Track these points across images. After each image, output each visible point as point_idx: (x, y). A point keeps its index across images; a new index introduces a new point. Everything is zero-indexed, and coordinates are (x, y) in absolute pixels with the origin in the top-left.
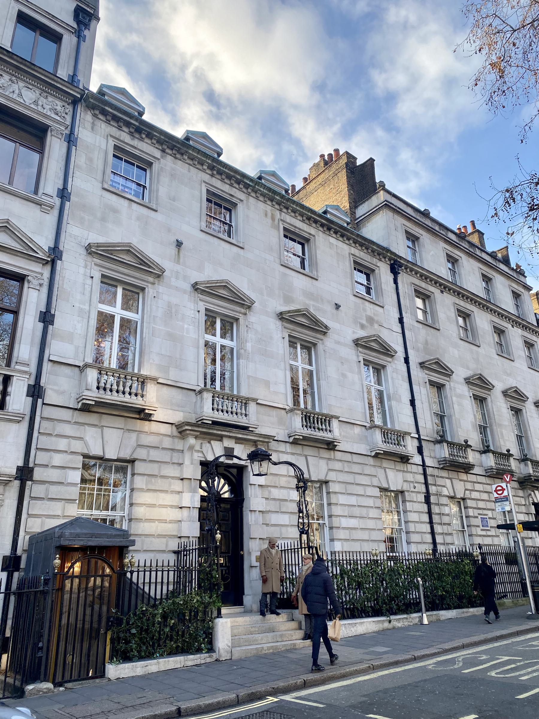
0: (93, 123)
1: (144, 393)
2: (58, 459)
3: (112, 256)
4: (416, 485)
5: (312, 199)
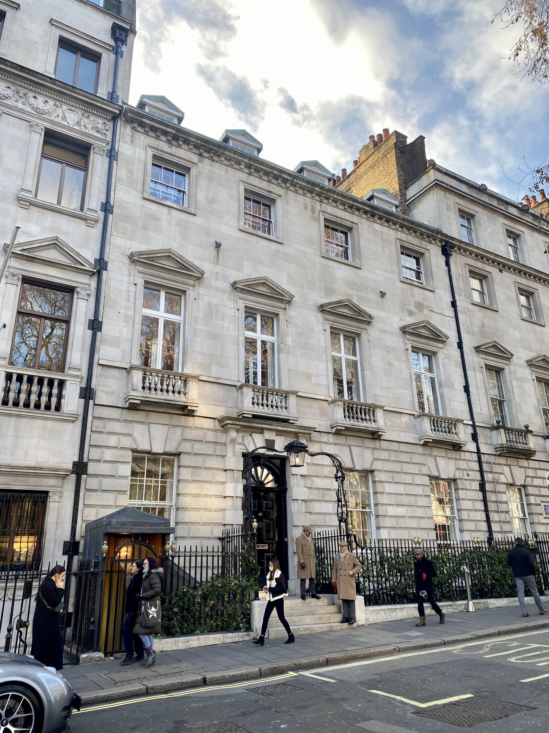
0: (132, 136)
1: (187, 391)
2: (109, 455)
3: (153, 263)
4: (470, 472)
5: (362, 183)
